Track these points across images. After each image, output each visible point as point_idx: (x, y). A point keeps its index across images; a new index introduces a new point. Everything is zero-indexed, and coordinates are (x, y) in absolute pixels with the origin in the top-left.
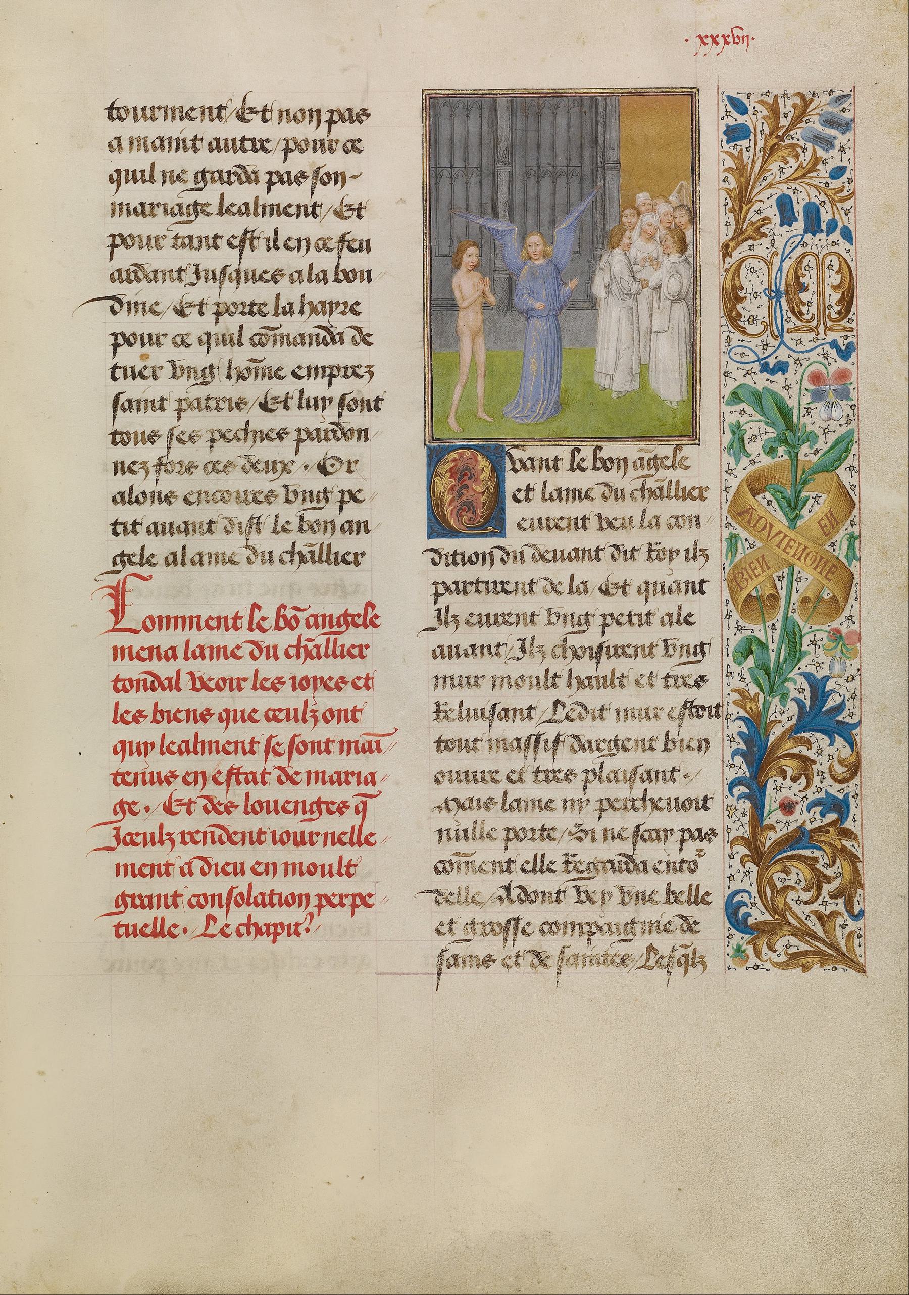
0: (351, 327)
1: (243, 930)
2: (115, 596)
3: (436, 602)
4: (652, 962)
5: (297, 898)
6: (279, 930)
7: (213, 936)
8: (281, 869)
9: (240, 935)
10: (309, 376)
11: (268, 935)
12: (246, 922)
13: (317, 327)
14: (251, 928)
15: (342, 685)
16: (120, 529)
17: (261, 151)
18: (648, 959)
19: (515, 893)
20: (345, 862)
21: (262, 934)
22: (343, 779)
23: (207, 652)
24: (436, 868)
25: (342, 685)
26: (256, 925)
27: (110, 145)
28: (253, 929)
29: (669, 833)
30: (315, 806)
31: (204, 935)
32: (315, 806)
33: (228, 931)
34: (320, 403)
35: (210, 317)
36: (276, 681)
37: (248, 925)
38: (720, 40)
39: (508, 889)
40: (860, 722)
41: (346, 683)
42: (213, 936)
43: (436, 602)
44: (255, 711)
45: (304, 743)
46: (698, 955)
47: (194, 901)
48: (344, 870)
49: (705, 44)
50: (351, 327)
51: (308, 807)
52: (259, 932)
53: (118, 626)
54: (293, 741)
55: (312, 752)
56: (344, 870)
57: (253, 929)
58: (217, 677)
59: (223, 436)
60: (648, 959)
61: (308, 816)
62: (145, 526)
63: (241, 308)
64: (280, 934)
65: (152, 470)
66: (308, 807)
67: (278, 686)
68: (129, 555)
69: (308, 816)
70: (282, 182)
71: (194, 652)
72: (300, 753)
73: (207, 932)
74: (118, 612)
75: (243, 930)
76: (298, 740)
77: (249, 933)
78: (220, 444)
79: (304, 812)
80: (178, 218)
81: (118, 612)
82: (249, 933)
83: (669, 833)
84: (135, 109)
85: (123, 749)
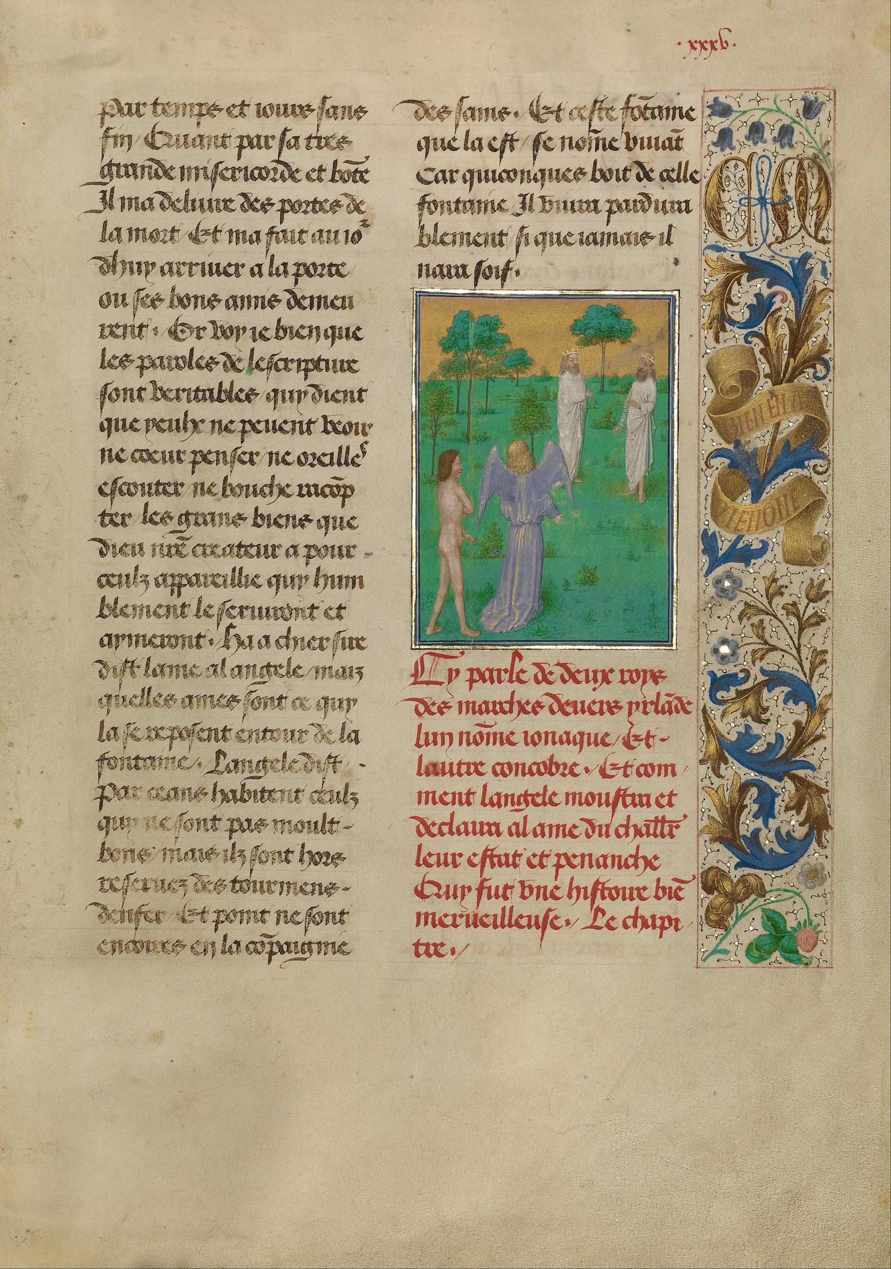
0: (412, 817)
1: (630, 922)
6: (666, 924)
7: (599, 928)
9: (626, 926)
11: (654, 927)
12: (633, 914)
13: (150, 160)
14: (638, 921)
15: (538, 709)
16: (422, 949)
17: (259, 180)
18: (595, 920)
21: (647, 927)
22: (175, 270)
24: (99, 580)
25: (538, 709)
26: (643, 917)
28: (639, 921)
29: (241, 331)
30: (522, 798)
31: (592, 927)
32: (522, 798)
33: (613, 924)
34: (295, 395)
35: (276, 216)
37: (635, 918)
38: (708, 46)
40: (699, 835)
42: (599, 928)
44: (136, 420)
46: (237, 849)
47: (137, 455)
49: (695, 49)
50: (412, 817)
51: (516, 800)
52: (645, 925)
57: (639, 921)
59: (205, 458)
60: (595, 920)
61: (516, 807)
62: (461, 174)
63: (324, 859)
64: (667, 928)
66: (516, 800)
69: (516, 807)
71: (458, 828)
75: (630, 922)
77: (635, 925)
78: (202, 467)
79: (513, 804)
80: (491, 730)
82: (635, 925)
83: (241, 331)
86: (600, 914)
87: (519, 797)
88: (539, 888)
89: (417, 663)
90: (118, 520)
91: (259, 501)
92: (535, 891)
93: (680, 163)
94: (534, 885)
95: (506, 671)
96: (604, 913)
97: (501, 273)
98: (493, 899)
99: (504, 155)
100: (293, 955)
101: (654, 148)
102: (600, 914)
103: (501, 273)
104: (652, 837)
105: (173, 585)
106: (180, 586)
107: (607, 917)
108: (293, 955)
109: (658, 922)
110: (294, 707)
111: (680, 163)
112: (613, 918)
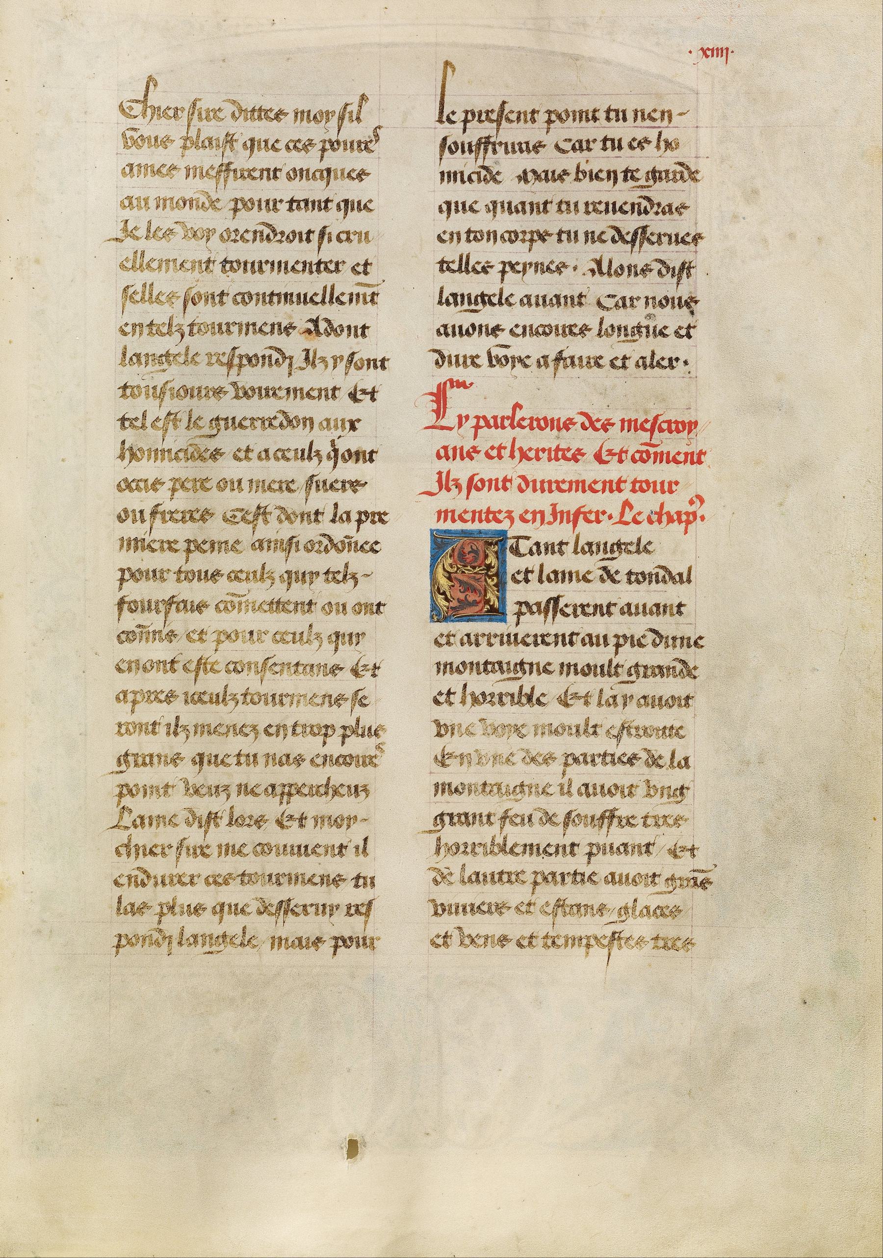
1: (655, 518)
2: (438, 402)
3: (120, 589)
4: (628, 517)
5: (571, 114)
7: (626, 523)
8: (582, 237)
9: (650, 522)
10: (304, 270)
11: (680, 522)
18: (121, 818)
19: (323, 326)
20: (614, 665)
23: (528, 208)
26: (668, 513)
27: (438, 331)
29: (464, 420)
33: (639, 518)
36: (471, 450)
37: (660, 514)
39: (315, 322)
41: (478, 452)
42: (626, 523)
43: (120, 589)
45: (482, 481)
48: (613, 671)
52: (670, 520)
53: (437, 424)
54: (471, 479)
55: (490, 489)
56: (613, 671)
58: (224, 873)
60: (121, 818)
65: (551, 364)
67: (473, 454)
68: (494, 513)
70: (489, 426)
72: (478, 489)
73: (624, 519)
74: (440, 412)
76: (476, 478)
81: (440, 412)
83: (464, 420)
84: (260, 201)
85: (289, 578)
86: (627, 509)
87: (476, 297)
88: (490, 481)
89: (443, 417)
90: (592, 517)
91: (556, 497)
92: (487, 484)
93: (325, 287)
94: (659, 786)
95: (508, 418)
96: (631, 507)
97: (571, 517)
98: (506, 645)
99: (180, 859)
100: (506, 676)
101: (539, 491)
102: (627, 509)
103: (571, 517)
104: (500, 429)
105: (282, 794)
106: (290, 794)
107: (635, 511)
108: (506, 676)
109: (684, 518)
110: (235, 302)
111: (325, 287)
112: (639, 513)
